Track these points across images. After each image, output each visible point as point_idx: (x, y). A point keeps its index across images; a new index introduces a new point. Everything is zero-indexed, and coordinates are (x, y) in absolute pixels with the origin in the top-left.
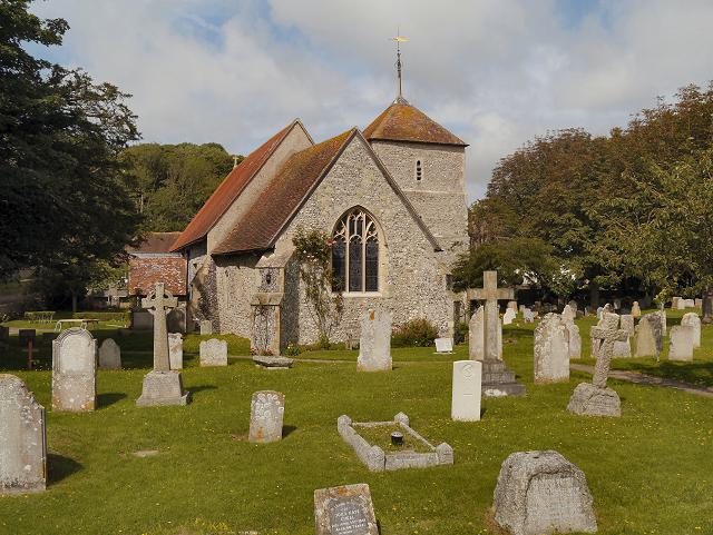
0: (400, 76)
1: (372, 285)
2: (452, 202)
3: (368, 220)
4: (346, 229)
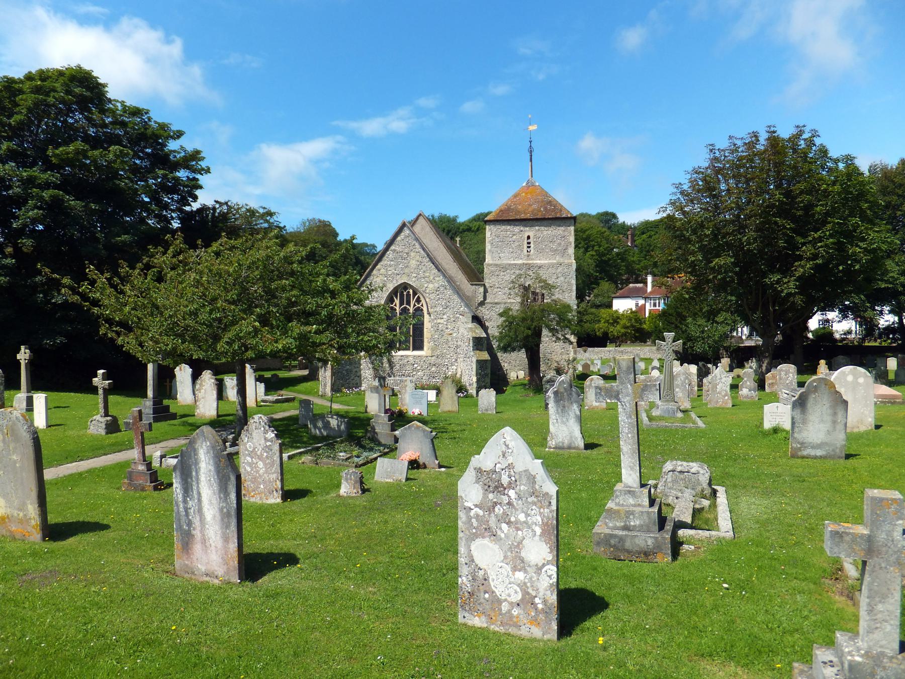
0: (531, 160)
1: (418, 346)
2: (560, 269)
3: (415, 293)
4: (397, 301)
